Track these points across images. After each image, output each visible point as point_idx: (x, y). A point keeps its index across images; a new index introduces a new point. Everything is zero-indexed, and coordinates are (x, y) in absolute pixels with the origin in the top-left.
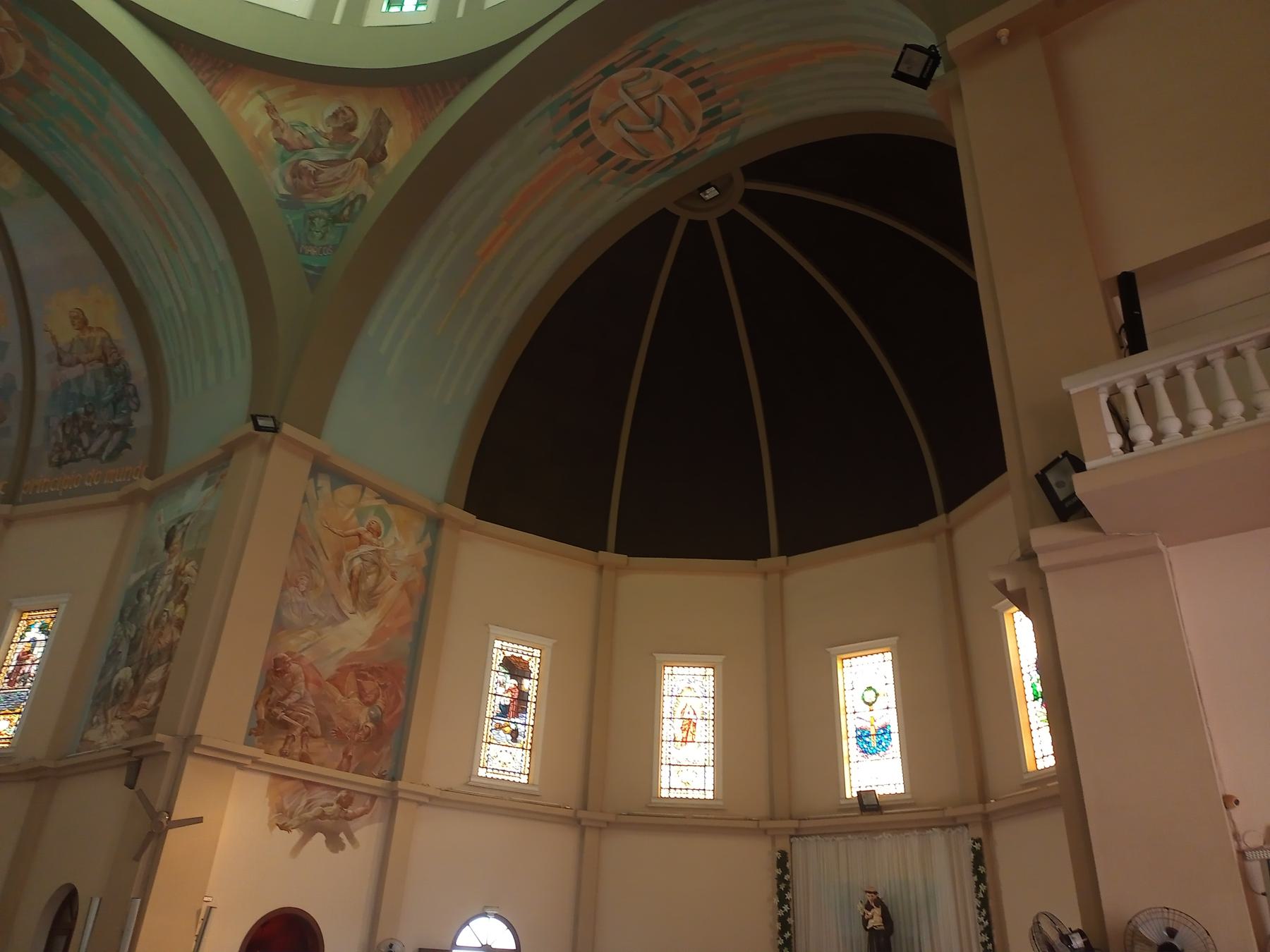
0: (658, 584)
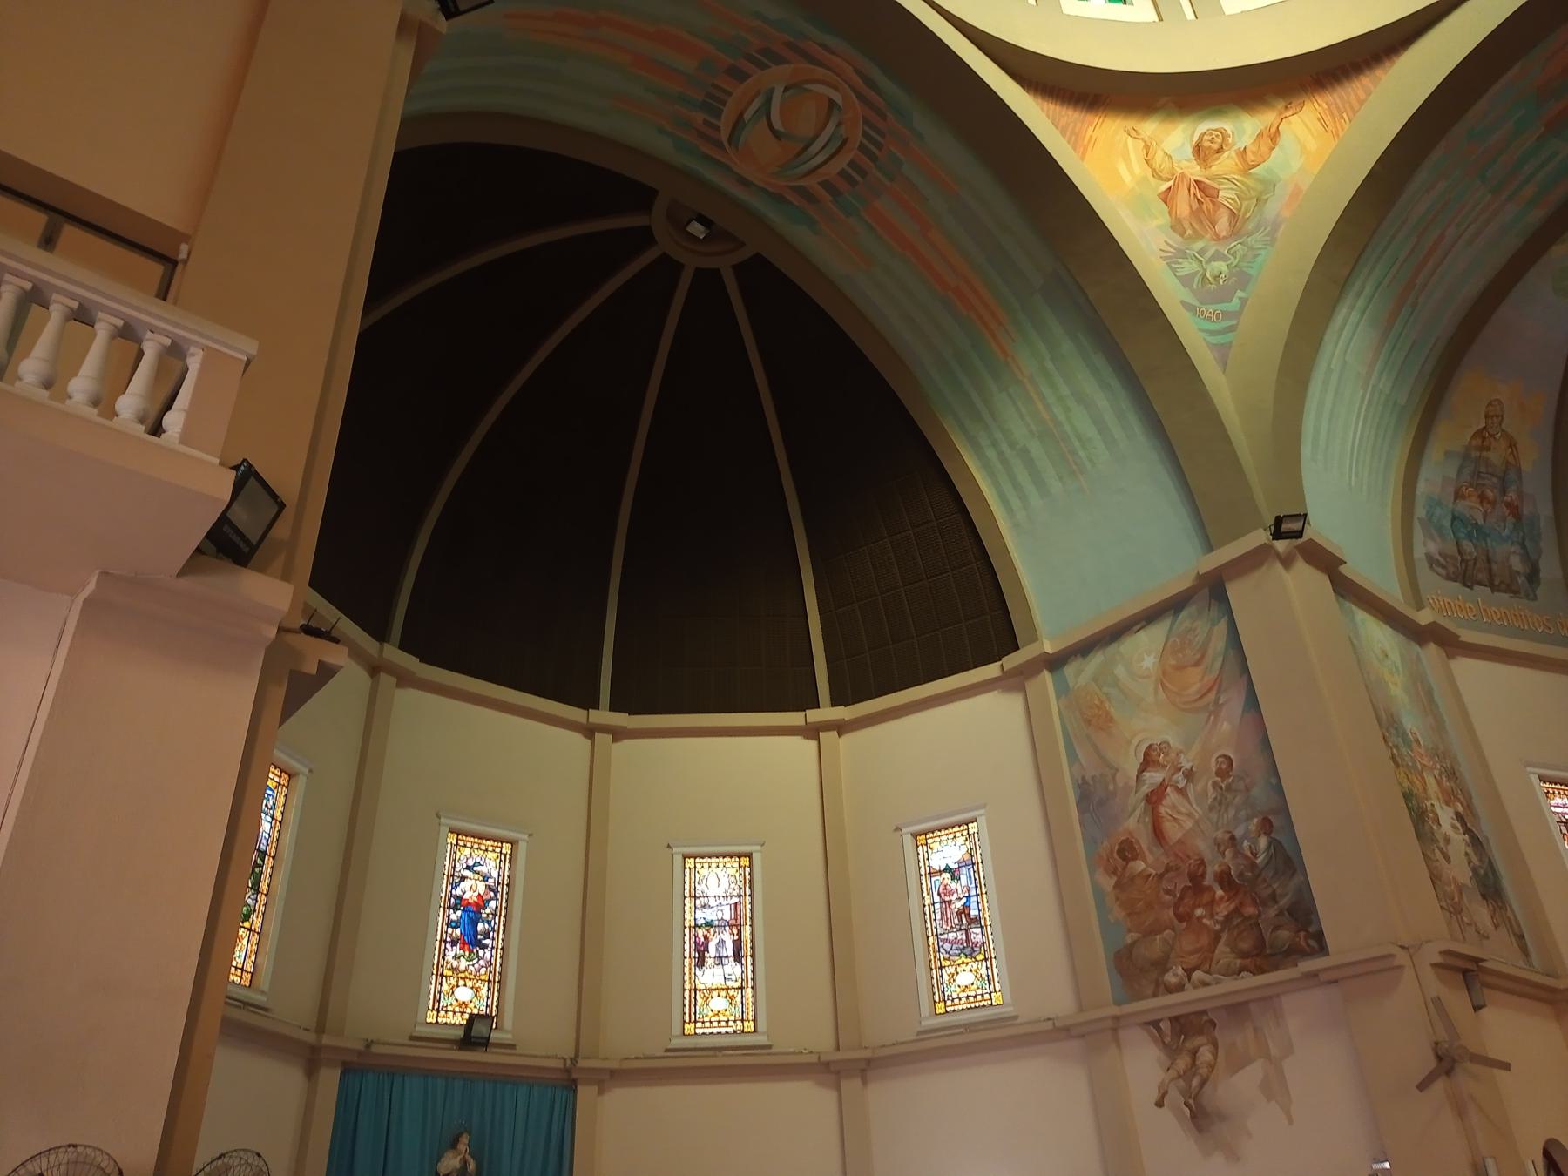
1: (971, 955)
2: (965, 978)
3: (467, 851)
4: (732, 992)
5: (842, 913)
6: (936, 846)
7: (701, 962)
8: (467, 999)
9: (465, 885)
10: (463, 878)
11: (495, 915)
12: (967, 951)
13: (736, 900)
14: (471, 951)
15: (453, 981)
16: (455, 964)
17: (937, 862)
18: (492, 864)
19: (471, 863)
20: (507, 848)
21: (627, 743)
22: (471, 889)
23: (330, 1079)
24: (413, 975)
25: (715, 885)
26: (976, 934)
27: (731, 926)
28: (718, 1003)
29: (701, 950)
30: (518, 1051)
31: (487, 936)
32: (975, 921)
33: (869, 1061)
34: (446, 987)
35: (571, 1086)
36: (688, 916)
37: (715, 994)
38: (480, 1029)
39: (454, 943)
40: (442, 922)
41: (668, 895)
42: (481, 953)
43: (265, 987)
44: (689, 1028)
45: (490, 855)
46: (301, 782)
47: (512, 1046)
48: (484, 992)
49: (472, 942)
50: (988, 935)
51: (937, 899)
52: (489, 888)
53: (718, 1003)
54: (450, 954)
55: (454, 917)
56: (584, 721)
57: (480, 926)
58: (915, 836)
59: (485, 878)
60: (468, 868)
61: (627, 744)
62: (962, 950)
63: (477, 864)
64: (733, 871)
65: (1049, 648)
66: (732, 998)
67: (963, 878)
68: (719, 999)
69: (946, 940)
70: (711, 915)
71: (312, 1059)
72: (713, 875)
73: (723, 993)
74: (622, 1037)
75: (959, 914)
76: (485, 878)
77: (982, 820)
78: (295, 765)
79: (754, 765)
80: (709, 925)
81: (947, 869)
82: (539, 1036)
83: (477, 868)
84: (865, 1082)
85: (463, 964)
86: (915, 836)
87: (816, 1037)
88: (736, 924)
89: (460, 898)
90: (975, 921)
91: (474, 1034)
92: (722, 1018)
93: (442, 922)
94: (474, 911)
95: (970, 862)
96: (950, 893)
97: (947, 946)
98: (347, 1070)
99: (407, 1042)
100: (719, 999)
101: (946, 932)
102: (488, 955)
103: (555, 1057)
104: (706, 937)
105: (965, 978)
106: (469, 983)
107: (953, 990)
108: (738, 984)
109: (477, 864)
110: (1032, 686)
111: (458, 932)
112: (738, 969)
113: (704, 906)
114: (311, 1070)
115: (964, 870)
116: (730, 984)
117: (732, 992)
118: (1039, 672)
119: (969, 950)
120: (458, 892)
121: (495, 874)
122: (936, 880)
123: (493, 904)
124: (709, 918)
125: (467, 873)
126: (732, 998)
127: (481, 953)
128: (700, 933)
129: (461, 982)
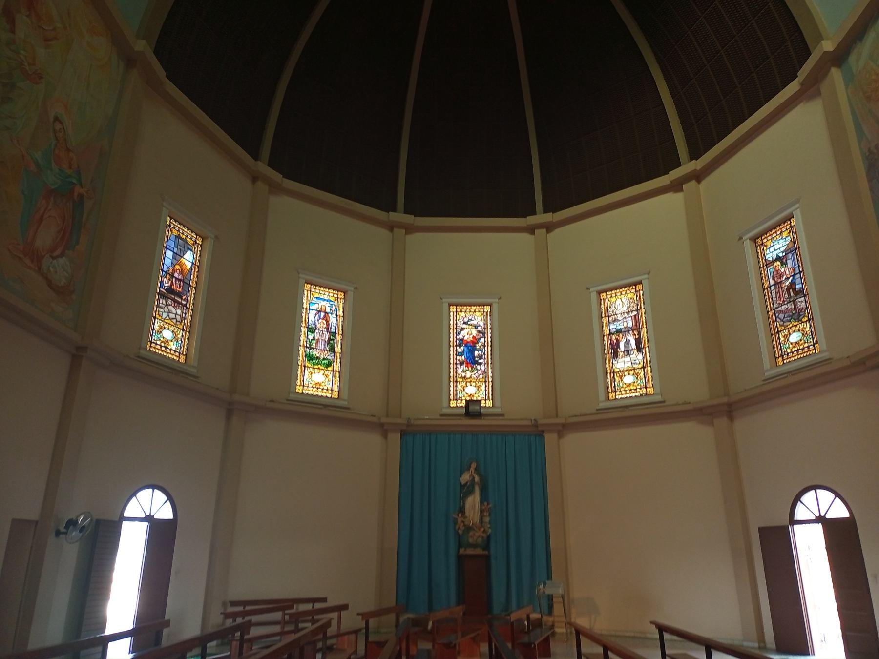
0: (304, 215)
1: (799, 319)
2: (795, 337)
3: (463, 314)
4: (637, 371)
5: (707, 310)
6: (769, 243)
7: (615, 355)
8: (473, 393)
9: (464, 333)
10: (462, 329)
11: (484, 346)
12: (795, 317)
13: (635, 313)
14: (472, 367)
15: (464, 384)
16: (463, 375)
17: (770, 255)
18: (479, 318)
19: (466, 320)
20: (487, 309)
21: (557, 231)
22: (468, 334)
23: (395, 438)
24: (441, 381)
25: (621, 305)
26: (801, 303)
27: (633, 330)
28: (629, 379)
29: (615, 347)
30: (506, 417)
31: (481, 357)
32: (800, 293)
33: (730, 405)
34: (459, 387)
35: (541, 434)
36: (605, 329)
37: (626, 373)
38: (472, 408)
39: (461, 364)
40: (456, 354)
41: (593, 316)
42: (478, 367)
43: (346, 397)
44: (612, 396)
45: (477, 314)
46: (350, 294)
47: (502, 415)
48: (483, 388)
49: (472, 362)
50: (812, 302)
51: (772, 282)
52: (479, 332)
53: (629, 379)
54: (460, 370)
55: (459, 350)
56: (525, 225)
57: (476, 353)
58: (754, 240)
59: (476, 327)
60: (465, 323)
61: (418, 236)
62: (792, 317)
63: (470, 320)
64: (629, 296)
65: (828, 46)
66: (638, 374)
67: (790, 263)
68: (630, 375)
69: (781, 312)
70: (619, 326)
71: (383, 429)
72: (619, 301)
73: (632, 373)
74: (572, 405)
75: (788, 290)
76: (476, 327)
77: (797, 214)
78: (347, 288)
79: (648, 219)
80: (619, 332)
81: (778, 258)
82: (527, 407)
83: (471, 322)
84: (731, 419)
85: (468, 374)
86: (754, 240)
87: (698, 392)
88: (637, 328)
89: (462, 340)
90: (800, 293)
91: (472, 409)
92: (632, 387)
93: (456, 354)
94: (471, 346)
95: (793, 249)
96: (781, 276)
97: (781, 316)
98: (404, 434)
99: (438, 417)
100: (630, 375)
101: (780, 305)
102: (483, 368)
103: (527, 419)
104: (617, 340)
105: (795, 337)
106: (474, 384)
107: (788, 348)
108: (640, 366)
109: (470, 320)
110: (824, 87)
111: (463, 358)
112: (640, 357)
113: (615, 321)
114: (385, 435)
115: (790, 256)
116: (635, 366)
117: (637, 371)
118: (827, 72)
119: (797, 315)
120: (461, 337)
121: (482, 324)
122: (770, 269)
123: (482, 340)
124: (618, 328)
125: (464, 326)
126: (638, 374)
127: (478, 367)
128: (614, 337)
129: (468, 384)
